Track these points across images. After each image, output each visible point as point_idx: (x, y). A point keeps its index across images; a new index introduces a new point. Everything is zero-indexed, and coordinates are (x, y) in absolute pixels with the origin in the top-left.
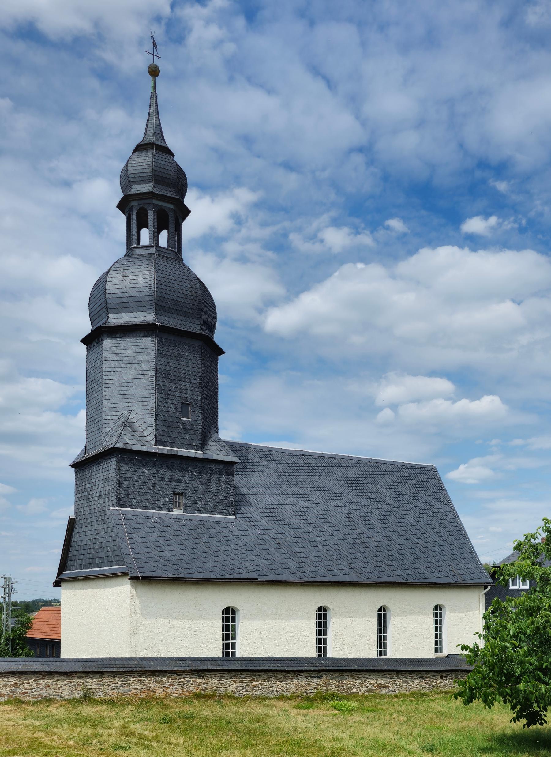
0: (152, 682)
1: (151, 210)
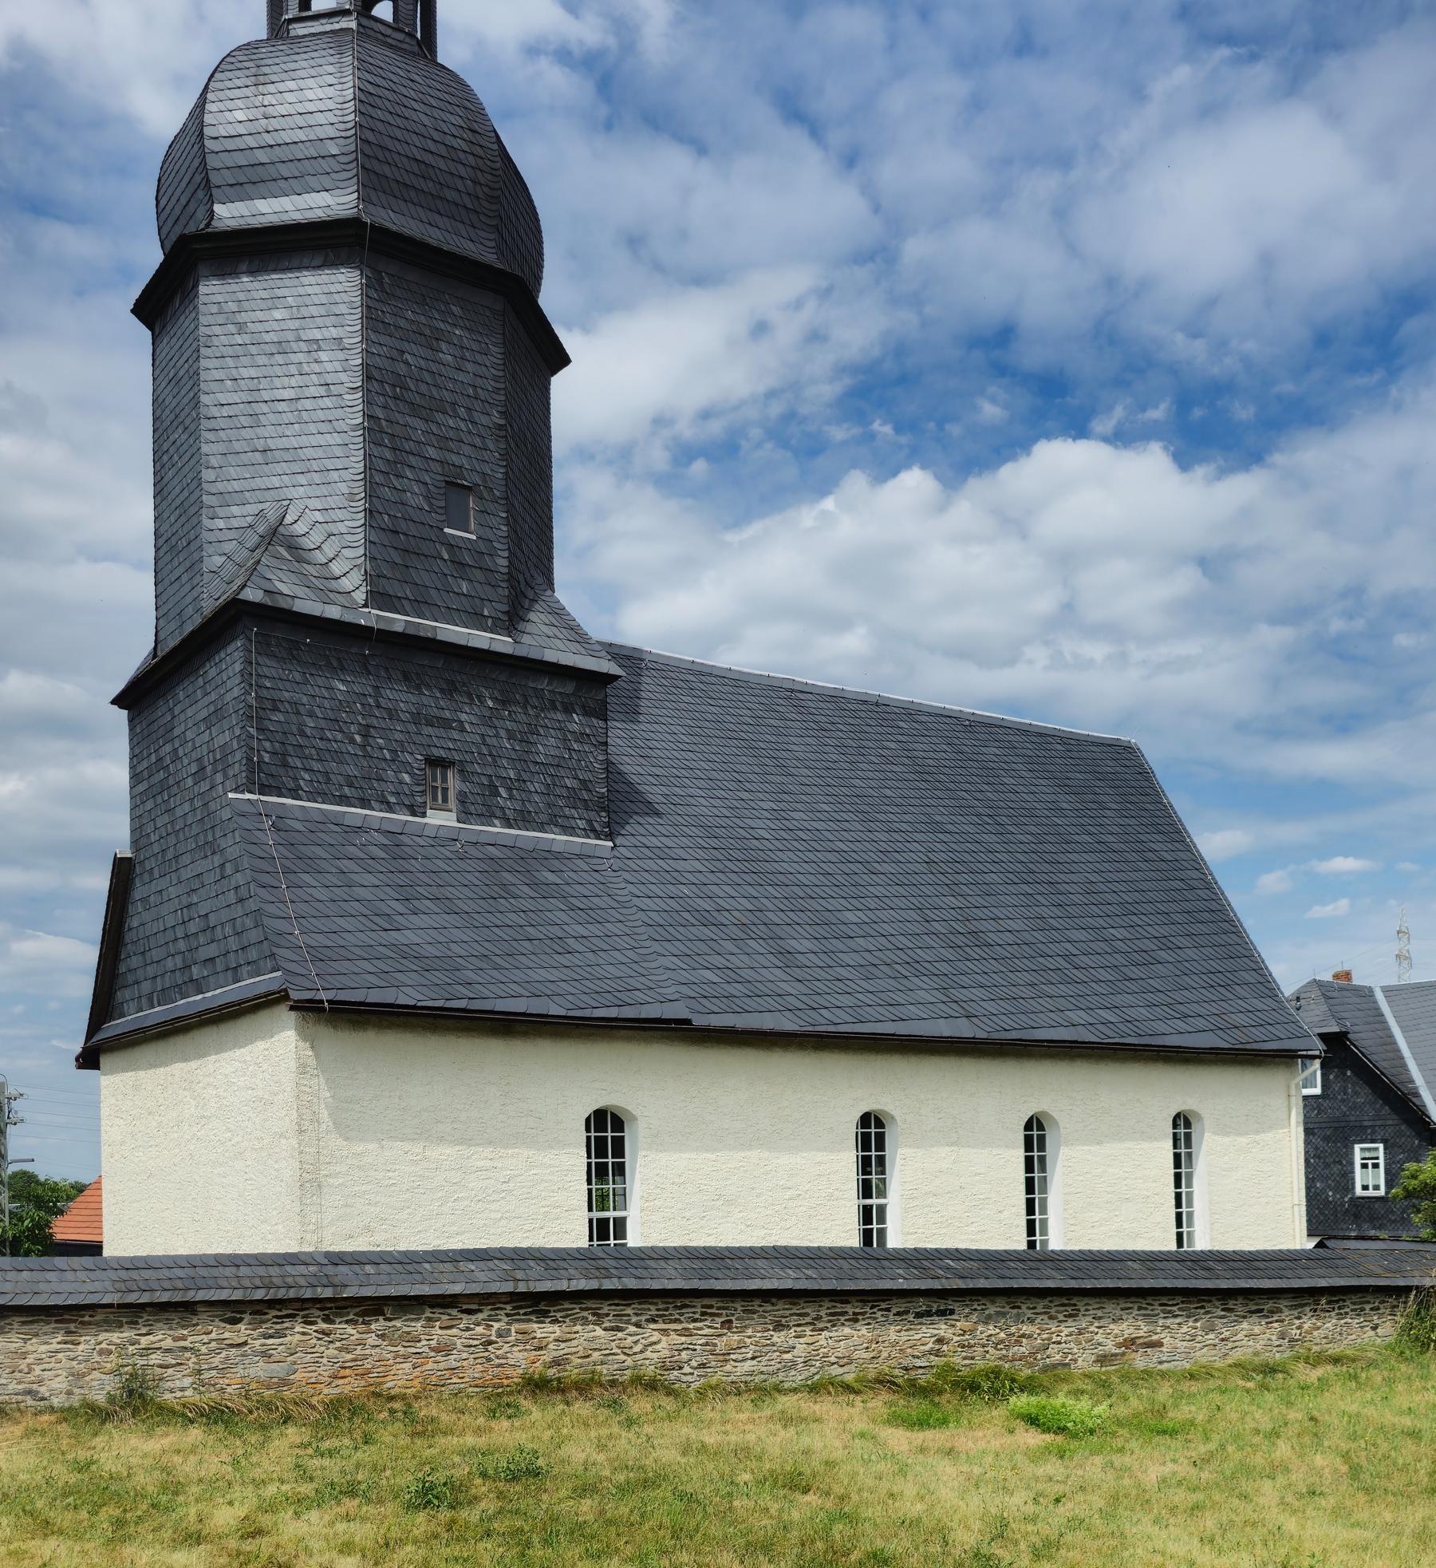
0: (372, 1339)
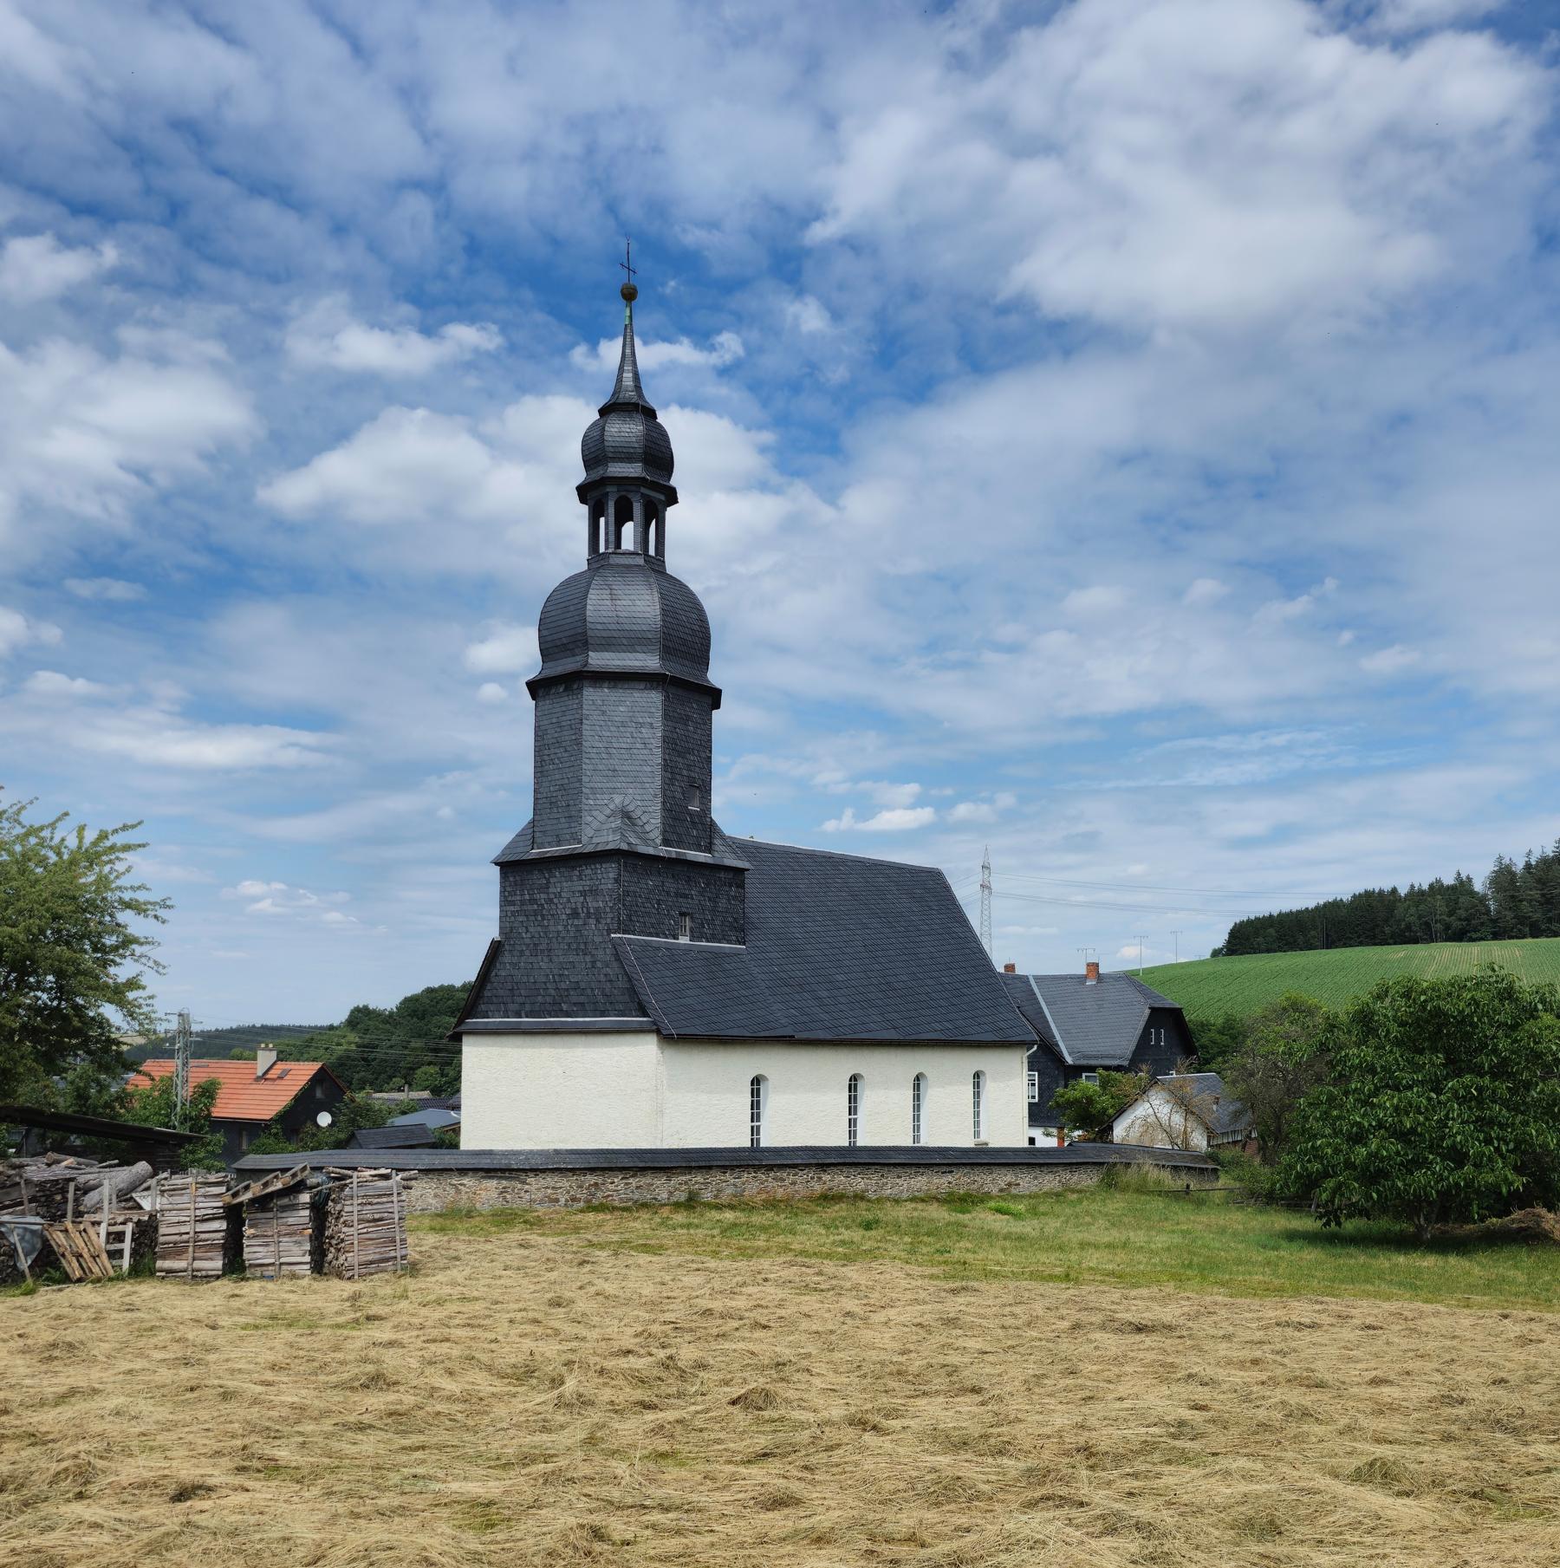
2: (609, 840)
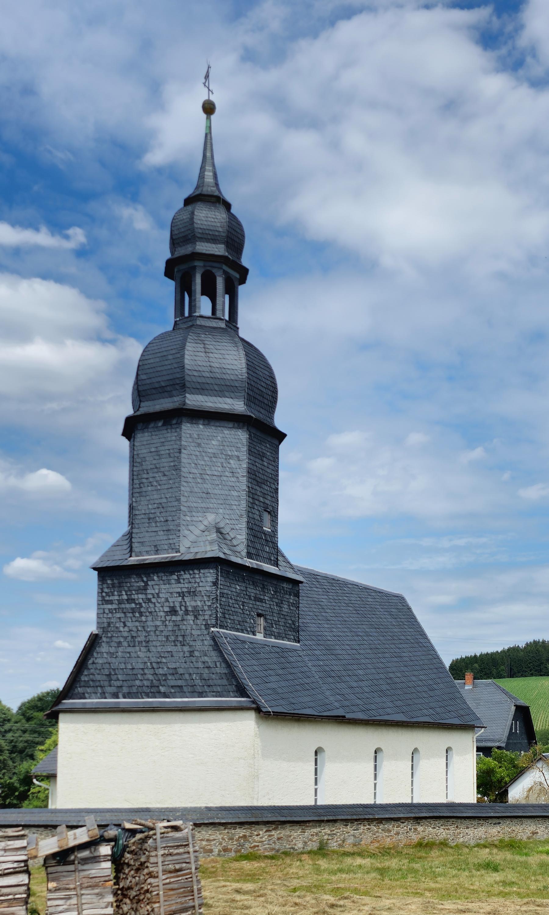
1: (220, 276)
2: (209, 549)
